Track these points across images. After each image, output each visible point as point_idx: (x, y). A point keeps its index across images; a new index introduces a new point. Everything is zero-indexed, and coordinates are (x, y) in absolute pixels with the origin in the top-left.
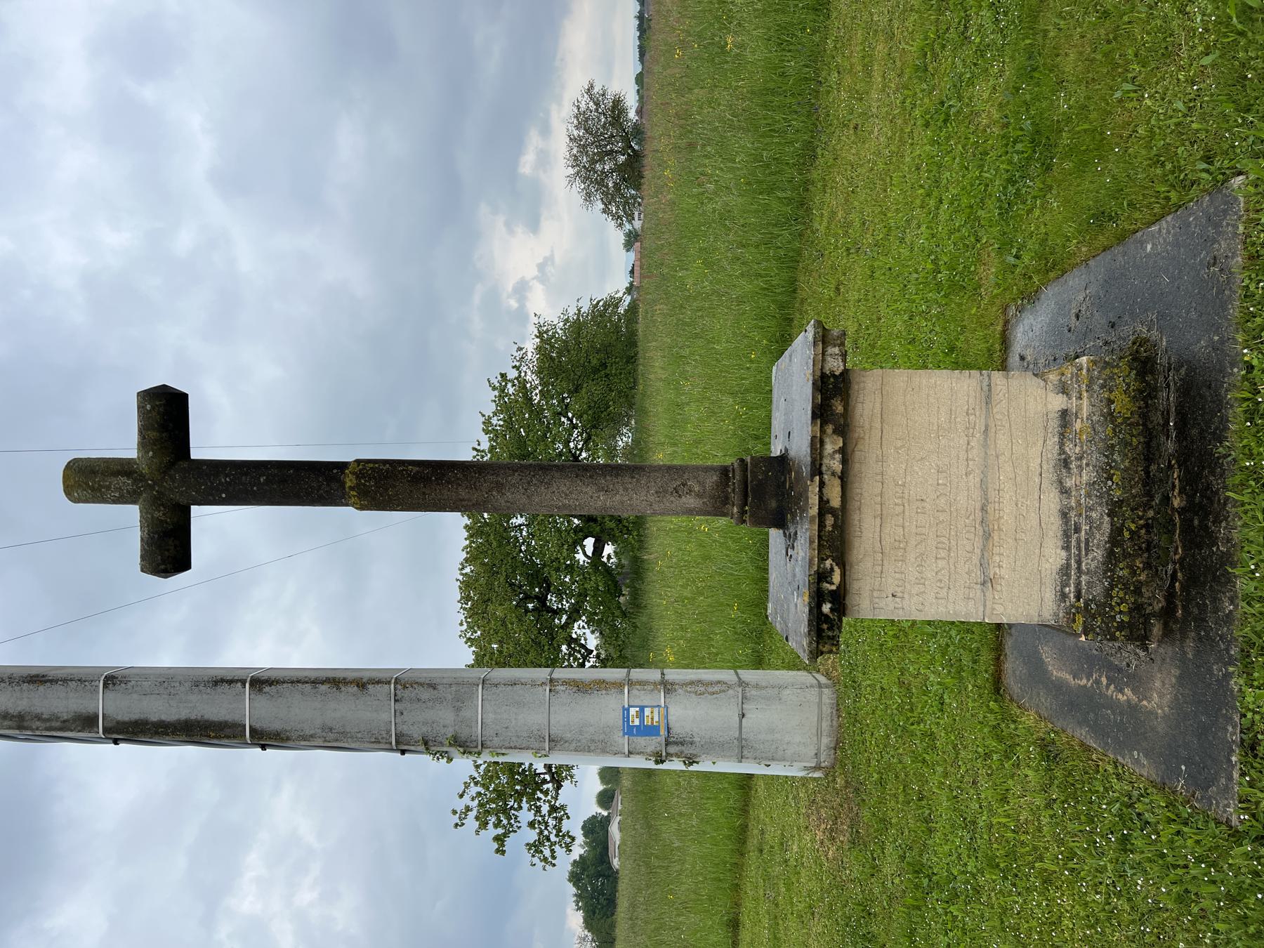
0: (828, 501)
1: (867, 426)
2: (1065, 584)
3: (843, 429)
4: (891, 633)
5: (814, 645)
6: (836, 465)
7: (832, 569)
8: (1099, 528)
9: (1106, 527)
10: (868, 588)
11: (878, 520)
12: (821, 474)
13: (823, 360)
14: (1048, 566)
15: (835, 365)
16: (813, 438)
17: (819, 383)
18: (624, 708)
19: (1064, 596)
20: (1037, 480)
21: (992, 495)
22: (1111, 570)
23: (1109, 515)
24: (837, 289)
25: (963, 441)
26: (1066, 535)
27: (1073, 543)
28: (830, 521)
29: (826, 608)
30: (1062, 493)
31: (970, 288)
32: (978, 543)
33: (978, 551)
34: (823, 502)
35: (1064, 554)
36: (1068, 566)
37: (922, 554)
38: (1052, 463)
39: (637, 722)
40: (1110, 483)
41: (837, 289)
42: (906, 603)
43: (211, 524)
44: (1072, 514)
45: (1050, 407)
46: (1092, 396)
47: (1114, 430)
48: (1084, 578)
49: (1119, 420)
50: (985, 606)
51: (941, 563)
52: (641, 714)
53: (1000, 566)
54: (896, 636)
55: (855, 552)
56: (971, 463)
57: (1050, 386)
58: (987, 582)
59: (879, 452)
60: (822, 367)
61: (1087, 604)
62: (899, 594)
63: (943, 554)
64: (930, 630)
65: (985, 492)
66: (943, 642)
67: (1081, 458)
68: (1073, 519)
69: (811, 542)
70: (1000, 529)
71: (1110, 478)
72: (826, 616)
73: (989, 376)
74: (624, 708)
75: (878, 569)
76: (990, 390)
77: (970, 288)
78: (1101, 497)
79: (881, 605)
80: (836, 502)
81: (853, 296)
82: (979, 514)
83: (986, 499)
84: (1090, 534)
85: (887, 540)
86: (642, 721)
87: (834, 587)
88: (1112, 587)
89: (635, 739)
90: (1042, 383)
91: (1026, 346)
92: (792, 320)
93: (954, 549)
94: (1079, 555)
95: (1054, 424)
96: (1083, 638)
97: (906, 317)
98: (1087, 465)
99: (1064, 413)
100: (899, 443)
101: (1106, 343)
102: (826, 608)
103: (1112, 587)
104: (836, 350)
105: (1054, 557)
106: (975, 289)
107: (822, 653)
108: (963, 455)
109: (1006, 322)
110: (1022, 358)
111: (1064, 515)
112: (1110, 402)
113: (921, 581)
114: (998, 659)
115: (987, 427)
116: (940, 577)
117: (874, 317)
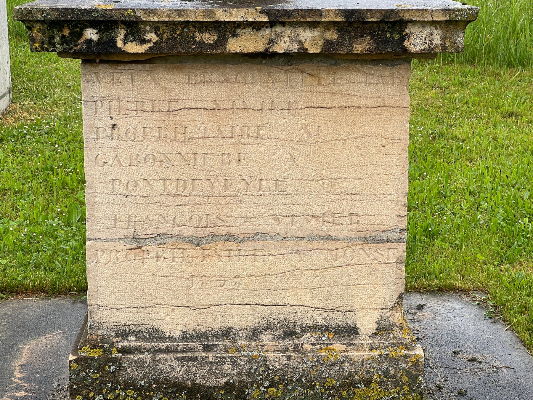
0: (235, 35)
1: (335, 89)
2: (139, 335)
3: (332, 57)
4: (68, 179)
5: (40, 17)
6: (281, 47)
7: (143, 42)
8: (211, 372)
9: (212, 381)
10: (122, 93)
11: (212, 105)
12: (271, 24)
13: (423, 24)
14: (161, 315)
15: (417, 40)
16: (319, 12)
17: (393, 19)
19: (124, 335)
20: (268, 301)
21: (249, 247)
22: (158, 388)
23: (227, 383)
24: (511, 114)
25: (317, 210)
26: (200, 336)
27: (191, 344)
28: (209, 38)
29: (91, 34)
30: (254, 330)
31: (509, 252)
32: (185, 232)
33: (176, 230)
34: (232, 28)
35: (177, 334)
36: (163, 339)
37: (169, 161)
38: (290, 318)
40: (267, 384)
41: (511, 114)
42: (107, 142)
44: (227, 343)
45: (361, 314)
46: (374, 361)
47: (333, 387)
48: (147, 357)
49: (344, 394)
50: (106, 240)
51: (159, 186)
53: (158, 257)
54: (64, 185)
55: (169, 76)
56: (289, 220)
57: (386, 314)
58: (138, 243)
59: (301, 105)
60: (414, 22)
61: (115, 360)
62: (115, 132)
63: (171, 188)
64: (75, 219)
65: (252, 238)
66: (61, 233)
67: (296, 349)
68: (221, 344)
69: (179, 12)
70: (205, 257)
71: (273, 384)
72: (80, 35)
73: (400, 240)
75: (148, 106)
76: (381, 241)
77: (509, 252)
78: (249, 374)
79: (100, 111)
80: (234, 45)
81: (502, 132)
82: (223, 231)
83: (242, 240)
84: (204, 362)
85: (185, 117)
87: (120, 44)
88: (137, 389)
90: (390, 304)
91: (435, 312)
92: (472, 63)
93: (178, 201)
94: (176, 351)
95: (340, 319)
96: (72, 357)
97: (473, 187)
98: (289, 358)
99: (353, 331)
100: (313, 130)
101: (439, 388)
102: (91, 34)
103: (137, 389)
104: (437, 41)
105: (173, 323)
106: (508, 259)
107: (30, 28)
108: (298, 210)
109: (465, 292)
110: (420, 308)
111: (226, 333)
112: (368, 383)
113: (134, 161)
114: (42, 290)
115: (332, 238)
116: (141, 183)
117: (474, 155)
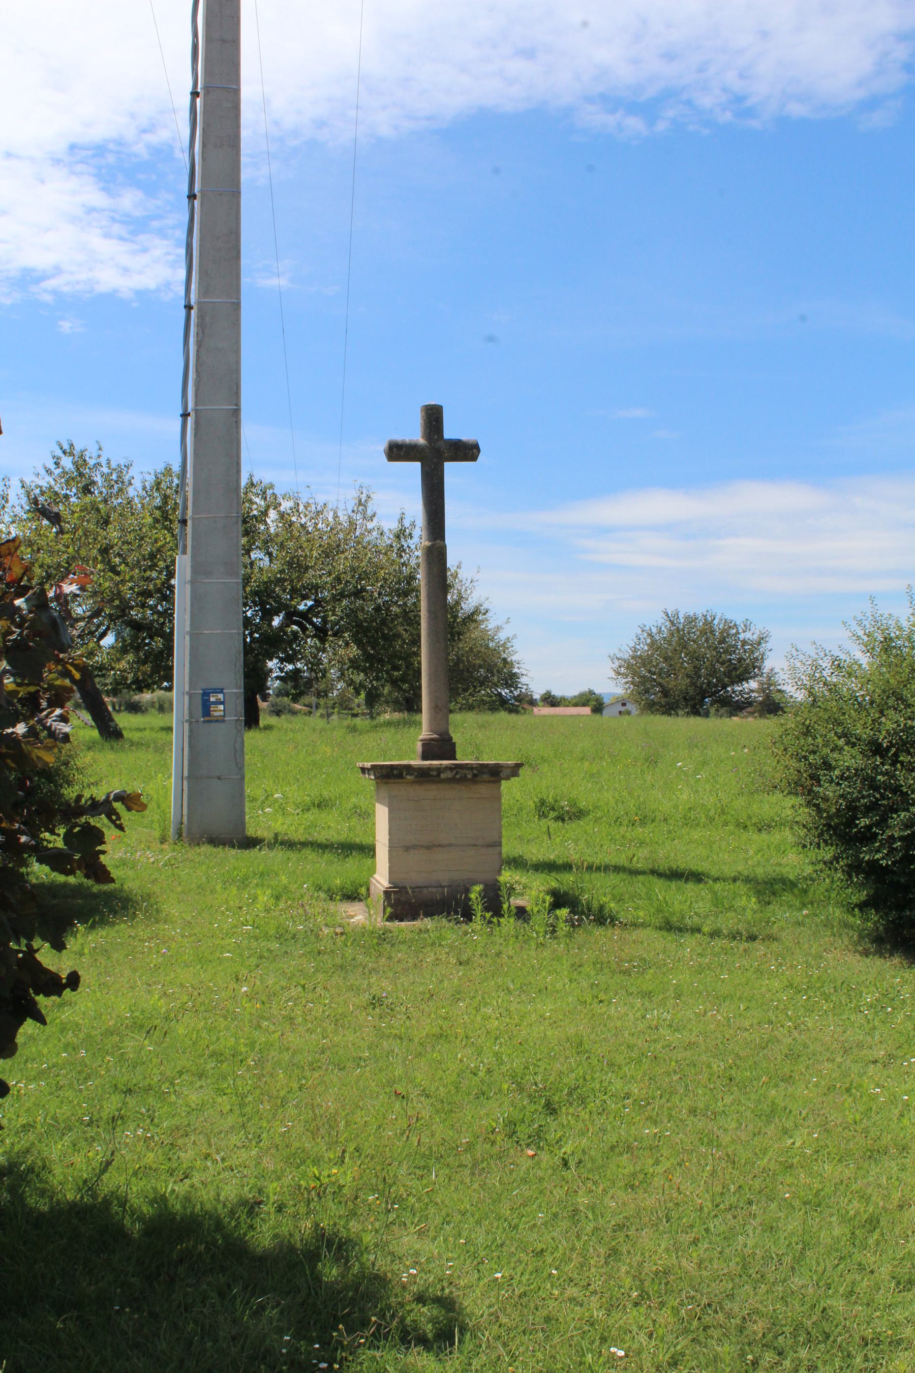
18: (222, 689)
39: (212, 699)
43: (414, 468)
52: (219, 702)
74: (222, 689)
86: (214, 703)
89: (200, 696)
